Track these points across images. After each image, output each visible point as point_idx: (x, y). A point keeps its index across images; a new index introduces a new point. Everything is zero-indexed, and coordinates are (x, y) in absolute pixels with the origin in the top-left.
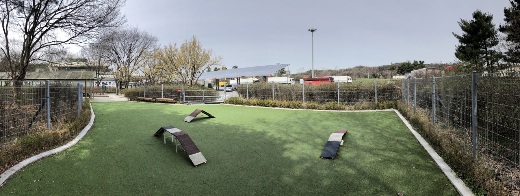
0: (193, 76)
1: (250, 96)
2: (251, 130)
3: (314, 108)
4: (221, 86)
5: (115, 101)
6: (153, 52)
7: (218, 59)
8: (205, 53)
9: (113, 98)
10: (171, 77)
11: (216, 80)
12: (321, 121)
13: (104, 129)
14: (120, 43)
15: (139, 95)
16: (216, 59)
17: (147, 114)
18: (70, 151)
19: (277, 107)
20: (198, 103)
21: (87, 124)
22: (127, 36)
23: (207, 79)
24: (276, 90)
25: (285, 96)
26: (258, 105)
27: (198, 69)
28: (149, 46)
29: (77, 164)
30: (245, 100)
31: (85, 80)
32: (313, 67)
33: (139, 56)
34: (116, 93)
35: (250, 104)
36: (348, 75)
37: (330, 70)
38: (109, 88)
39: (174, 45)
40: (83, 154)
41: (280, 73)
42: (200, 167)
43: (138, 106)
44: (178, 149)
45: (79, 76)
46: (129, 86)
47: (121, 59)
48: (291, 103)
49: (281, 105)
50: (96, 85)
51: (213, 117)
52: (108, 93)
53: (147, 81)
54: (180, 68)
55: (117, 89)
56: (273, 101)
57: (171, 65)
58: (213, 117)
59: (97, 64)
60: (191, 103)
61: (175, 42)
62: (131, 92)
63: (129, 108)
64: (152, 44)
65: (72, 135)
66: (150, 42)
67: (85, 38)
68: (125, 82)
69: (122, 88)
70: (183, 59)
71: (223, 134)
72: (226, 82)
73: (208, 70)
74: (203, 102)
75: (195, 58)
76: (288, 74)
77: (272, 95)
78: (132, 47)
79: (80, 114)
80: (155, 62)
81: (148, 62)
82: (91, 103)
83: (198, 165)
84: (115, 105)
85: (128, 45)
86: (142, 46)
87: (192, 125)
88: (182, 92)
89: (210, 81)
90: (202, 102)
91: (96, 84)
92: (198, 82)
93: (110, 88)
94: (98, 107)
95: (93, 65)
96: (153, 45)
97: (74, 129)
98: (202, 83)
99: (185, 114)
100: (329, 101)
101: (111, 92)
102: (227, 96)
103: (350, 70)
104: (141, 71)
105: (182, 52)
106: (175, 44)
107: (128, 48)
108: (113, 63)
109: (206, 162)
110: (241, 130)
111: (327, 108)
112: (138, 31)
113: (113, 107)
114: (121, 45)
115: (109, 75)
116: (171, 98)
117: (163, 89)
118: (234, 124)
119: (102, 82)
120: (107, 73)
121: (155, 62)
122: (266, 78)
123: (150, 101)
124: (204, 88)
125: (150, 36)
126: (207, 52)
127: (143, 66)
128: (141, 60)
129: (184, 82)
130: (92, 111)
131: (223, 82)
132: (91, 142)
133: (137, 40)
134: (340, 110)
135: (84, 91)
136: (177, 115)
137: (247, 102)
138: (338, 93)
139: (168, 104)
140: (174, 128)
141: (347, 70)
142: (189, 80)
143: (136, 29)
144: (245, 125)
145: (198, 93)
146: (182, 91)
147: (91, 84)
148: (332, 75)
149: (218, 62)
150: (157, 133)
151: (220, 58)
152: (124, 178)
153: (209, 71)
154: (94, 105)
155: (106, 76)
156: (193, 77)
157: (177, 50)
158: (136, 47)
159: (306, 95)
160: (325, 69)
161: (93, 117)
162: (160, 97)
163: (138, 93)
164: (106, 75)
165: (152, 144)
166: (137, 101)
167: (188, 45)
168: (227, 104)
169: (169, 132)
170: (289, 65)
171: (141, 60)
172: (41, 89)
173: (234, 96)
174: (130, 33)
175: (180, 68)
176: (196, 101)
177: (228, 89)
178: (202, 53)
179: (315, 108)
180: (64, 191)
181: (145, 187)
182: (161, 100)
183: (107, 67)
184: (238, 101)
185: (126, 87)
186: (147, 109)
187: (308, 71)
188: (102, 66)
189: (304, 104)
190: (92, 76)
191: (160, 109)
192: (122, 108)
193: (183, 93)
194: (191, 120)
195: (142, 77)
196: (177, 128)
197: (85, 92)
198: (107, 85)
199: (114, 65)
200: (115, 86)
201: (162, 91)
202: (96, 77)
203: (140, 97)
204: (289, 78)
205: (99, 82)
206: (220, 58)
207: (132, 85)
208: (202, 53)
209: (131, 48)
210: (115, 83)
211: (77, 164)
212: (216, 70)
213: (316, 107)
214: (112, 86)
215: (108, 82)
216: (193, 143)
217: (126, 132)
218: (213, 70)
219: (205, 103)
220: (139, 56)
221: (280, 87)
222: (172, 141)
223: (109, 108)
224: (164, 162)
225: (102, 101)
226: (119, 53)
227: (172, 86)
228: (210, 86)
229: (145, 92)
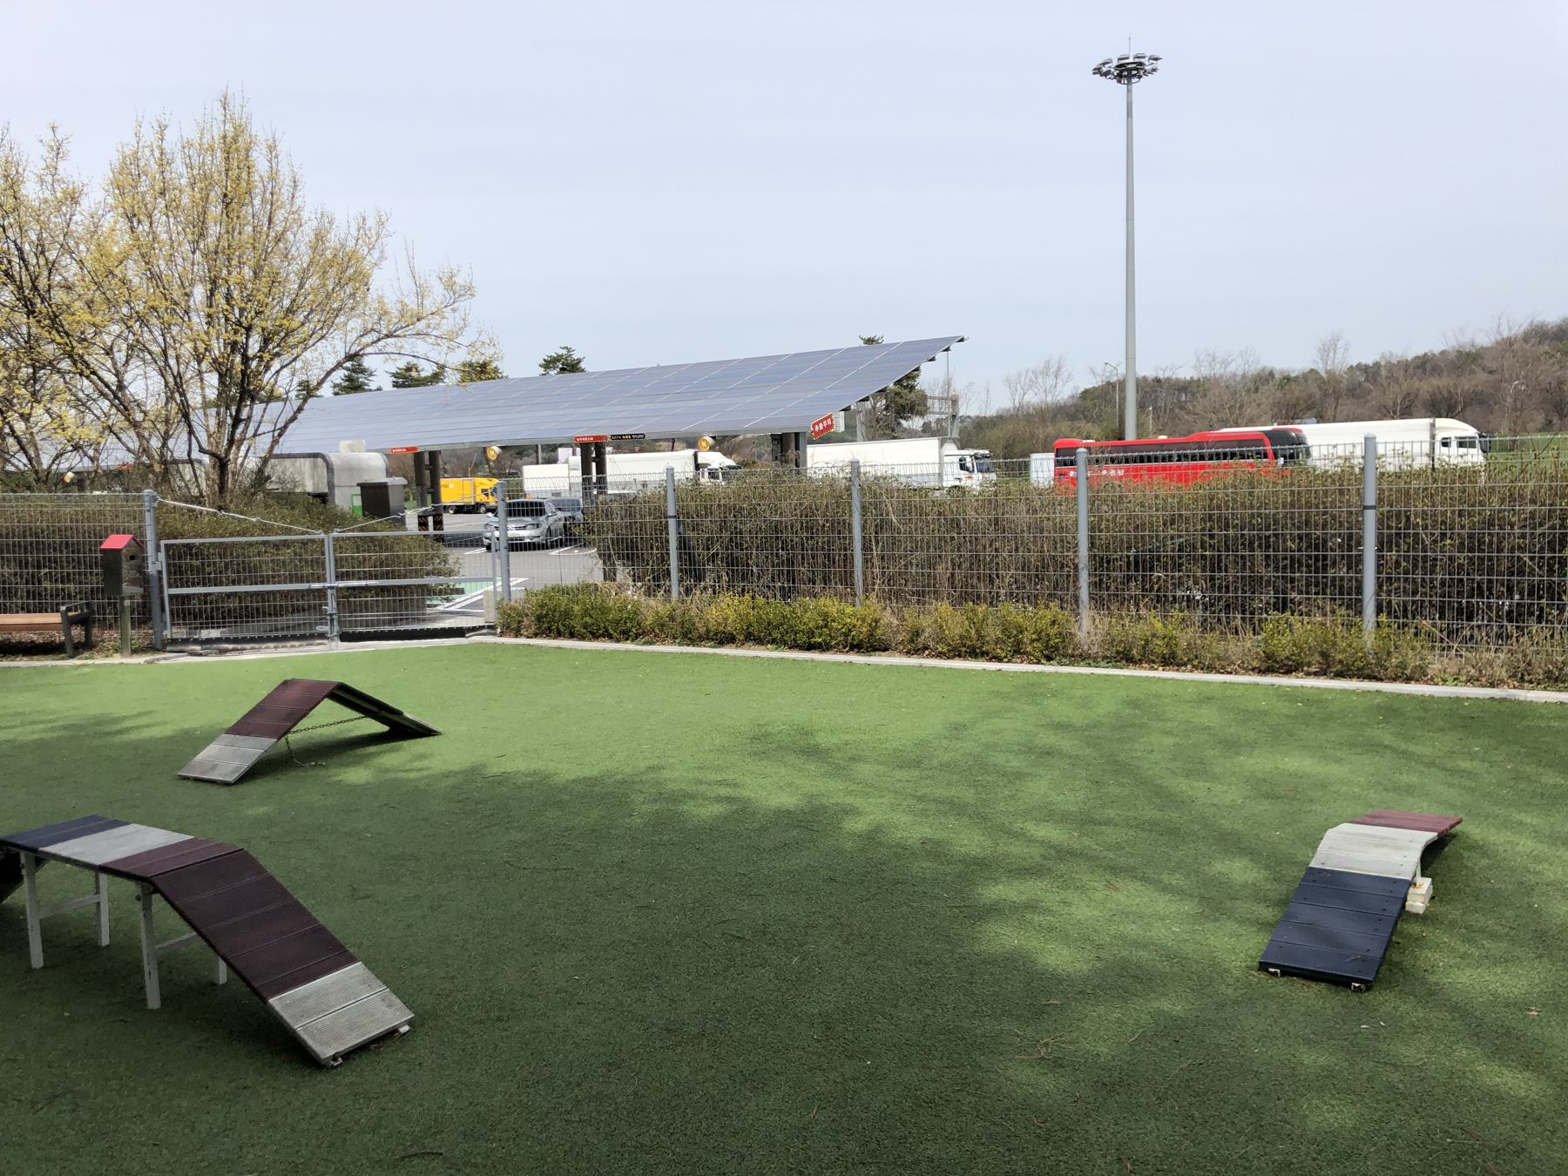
0: (237, 421)
1: (693, 572)
2: (719, 799)
3: (1169, 661)
4: (460, 510)
7: (437, 294)
8: (333, 240)
11: (418, 456)
12: (1231, 746)
16: (421, 294)
19: (885, 650)
20: (285, 639)
23: (352, 448)
24: (879, 528)
25: (942, 570)
26: (752, 637)
27: (276, 365)
30: (653, 607)
32: (1130, 357)
35: (695, 635)
36: (1440, 407)
37: (1265, 378)
39: (44, 151)
41: (887, 408)
42: (362, 1062)
48: (998, 616)
49: (917, 633)
51: (424, 732)
54: (109, 352)
56: (859, 610)
57: (20, 318)
58: (424, 732)
60: (227, 640)
70: (133, 271)
71: (517, 836)
73: (349, 379)
75: (247, 272)
76: (938, 421)
77: (848, 560)
83: (349, 1055)
87: (259, 802)
88: (137, 554)
89: (374, 467)
90: (321, 629)
92: (276, 469)
98: (309, 481)
99: (186, 726)
100: (1282, 605)
102: (514, 581)
103: (1465, 360)
106: (58, 151)
109: (409, 1022)
110: (646, 808)
111: (1269, 656)
118: (588, 772)
122: (786, 445)
124: (334, 520)
126: (342, 232)
131: (474, 474)
134: (1381, 680)
137: (672, 618)
138: (1359, 543)
140: (128, 823)
141: (1424, 365)
144: (666, 774)
146: (140, 544)
148: (1294, 412)
149: (435, 320)
151: (450, 285)
153: (353, 386)
156: (235, 426)
157: (73, 198)
159: (1100, 563)
160: (1232, 368)
167: (179, 166)
168: (522, 641)
170: (955, 346)
173: (571, 580)
175: (109, 352)
176: (270, 622)
178: (307, 233)
179: (1173, 655)
184: (604, 610)
187: (1089, 386)
189: (1088, 626)
193: (156, 563)
196: (141, 823)
204: (951, 448)
206: (457, 290)
208: (301, 244)
213: (1179, 653)
216: (302, 911)
218: (387, 383)
219: (345, 637)
221: (905, 509)
222: (98, 933)
228: (375, 499)
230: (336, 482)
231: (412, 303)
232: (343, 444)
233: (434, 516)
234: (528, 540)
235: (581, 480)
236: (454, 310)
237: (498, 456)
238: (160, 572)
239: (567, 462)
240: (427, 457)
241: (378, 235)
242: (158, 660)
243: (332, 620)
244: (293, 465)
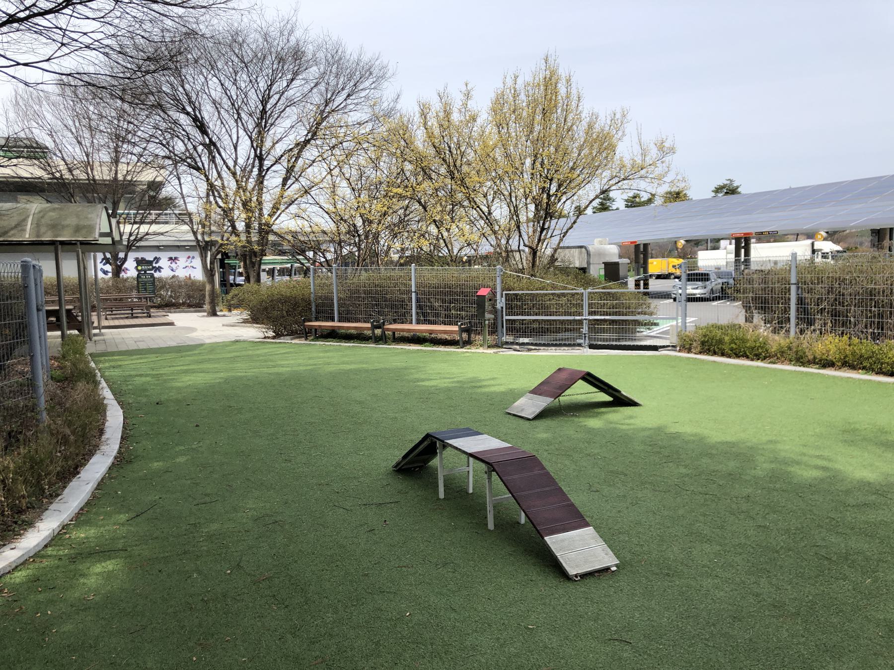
0: (543, 229)
4: (659, 277)
5: (208, 341)
6: (369, 127)
7: (654, 152)
9: (193, 330)
10: (445, 234)
11: (637, 247)
13: (178, 460)
14: (213, 82)
15: (313, 309)
16: (644, 155)
17: (355, 388)
18: (18, 580)
20: (560, 345)
21: (91, 454)
22: (248, 55)
28: (349, 101)
29: (68, 627)
31: (52, 248)
33: (307, 142)
34: (207, 307)
38: (171, 286)
39: (462, 97)
40: (92, 581)
43: (310, 358)
44: (495, 517)
45: (20, 225)
46: (264, 276)
47: (223, 154)
50: (105, 272)
51: (632, 403)
52: (170, 305)
53: (345, 252)
54: (485, 196)
55: (208, 287)
57: (448, 181)
58: (632, 403)
59: (102, 173)
60: (532, 344)
61: (466, 85)
62: (279, 300)
63: (274, 367)
64: (363, 94)
65: (20, 512)
66: (352, 84)
67: (44, 48)
68: (244, 257)
69: (232, 285)
70: (498, 154)
72: (680, 257)
73: (602, 204)
74: (581, 341)
78: (272, 101)
79: (49, 411)
80: (376, 167)
81: (346, 170)
82: (91, 355)
84: (209, 361)
85: (252, 94)
86: (316, 98)
87: (543, 431)
88: (493, 299)
89: (612, 253)
90: (579, 341)
91: (108, 268)
92: (560, 254)
93: (175, 285)
94: (133, 373)
95: (83, 176)
96: (367, 98)
97: (25, 482)
98: (577, 260)
101: (183, 304)
102: (689, 320)
104: (316, 208)
105: (495, 130)
106: (468, 95)
107: (254, 100)
108: (184, 168)
112: (298, 34)
113: (201, 366)
114: (219, 88)
115: (167, 223)
116: (450, 324)
117: (416, 286)
119: (132, 256)
120: (159, 215)
121: (376, 167)
123: (360, 337)
125: (355, 57)
127: (324, 185)
128: (314, 161)
129: (505, 256)
130: (107, 394)
131: (668, 257)
132: (123, 525)
133: (296, 74)
135: (53, 302)
136: (479, 390)
139: (435, 348)
140: (478, 433)
142: (522, 247)
143: (289, 26)
145: (563, 300)
146: (494, 294)
147: (82, 269)
150: (405, 457)
151: (661, 147)
152: (294, 635)
153: (603, 208)
154: (107, 365)
155: (155, 228)
156: (541, 232)
157: (474, 119)
158: (291, 103)
161: (115, 418)
162: (403, 318)
163: (310, 304)
164: (151, 223)
165: (388, 501)
166: (306, 339)
169: (460, 450)
171: (314, 161)
174: (261, 40)
175: (485, 196)
181: (379, 656)
182: (409, 331)
183: (155, 186)
184: (744, 341)
185: (252, 280)
186: (350, 370)
188: (132, 184)
190: (91, 229)
191: (406, 368)
192: (243, 370)
193: (501, 303)
194: (538, 411)
195: (324, 232)
197: (57, 308)
198: (159, 269)
199: (189, 178)
200: (198, 274)
201: (410, 292)
202: (109, 234)
203: (317, 319)
205: (121, 255)
207: (273, 269)
209: (269, 106)
210: (197, 262)
211: (68, 627)
212: (633, 203)
214: (182, 273)
215: (164, 257)
217: (277, 466)
219: (592, 347)
220: (307, 142)
223: (186, 372)
224: (445, 565)
225: (142, 346)
226: (213, 125)
227: (452, 274)
228: (612, 271)
229: (339, 299)
230: (591, 262)
231: (639, 161)
234: (699, 296)
235: (734, 260)
236: (662, 162)
238: (502, 308)
239: (725, 248)
240: (642, 246)
241: (622, 122)
244: (570, 253)
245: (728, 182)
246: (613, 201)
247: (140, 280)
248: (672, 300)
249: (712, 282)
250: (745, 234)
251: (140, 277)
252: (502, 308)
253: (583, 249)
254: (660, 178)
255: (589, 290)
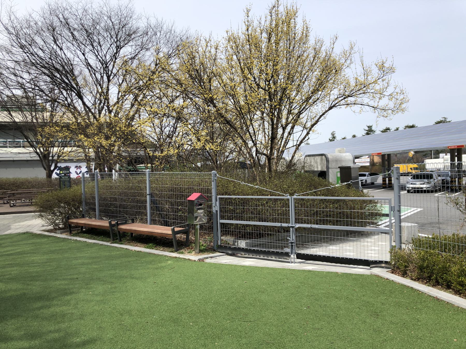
7: (375, 72)
16: (366, 73)
23: (340, 152)
151: (381, 67)
168: (407, 282)
172: (204, 190)
177: (418, 184)
180: (203, 323)
230: (330, 166)
231: (362, 79)
232: (337, 150)
233: (389, 178)
234: (425, 189)
235: (449, 164)
236: (383, 81)
237: (413, 155)
238: (217, 211)
239: (443, 158)
240: (386, 156)
241: (350, 53)
242: (207, 258)
243: (292, 246)
244: (314, 159)
245: (443, 119)
246: (375, 132)
247: (61, 180)
248: (406, 192)
249: (434, 179)
250: (458, 146)
251: (62, 178)
252: (217, 211)
253: (324, 157)
254: (381, 93)
255: (295, 197)
